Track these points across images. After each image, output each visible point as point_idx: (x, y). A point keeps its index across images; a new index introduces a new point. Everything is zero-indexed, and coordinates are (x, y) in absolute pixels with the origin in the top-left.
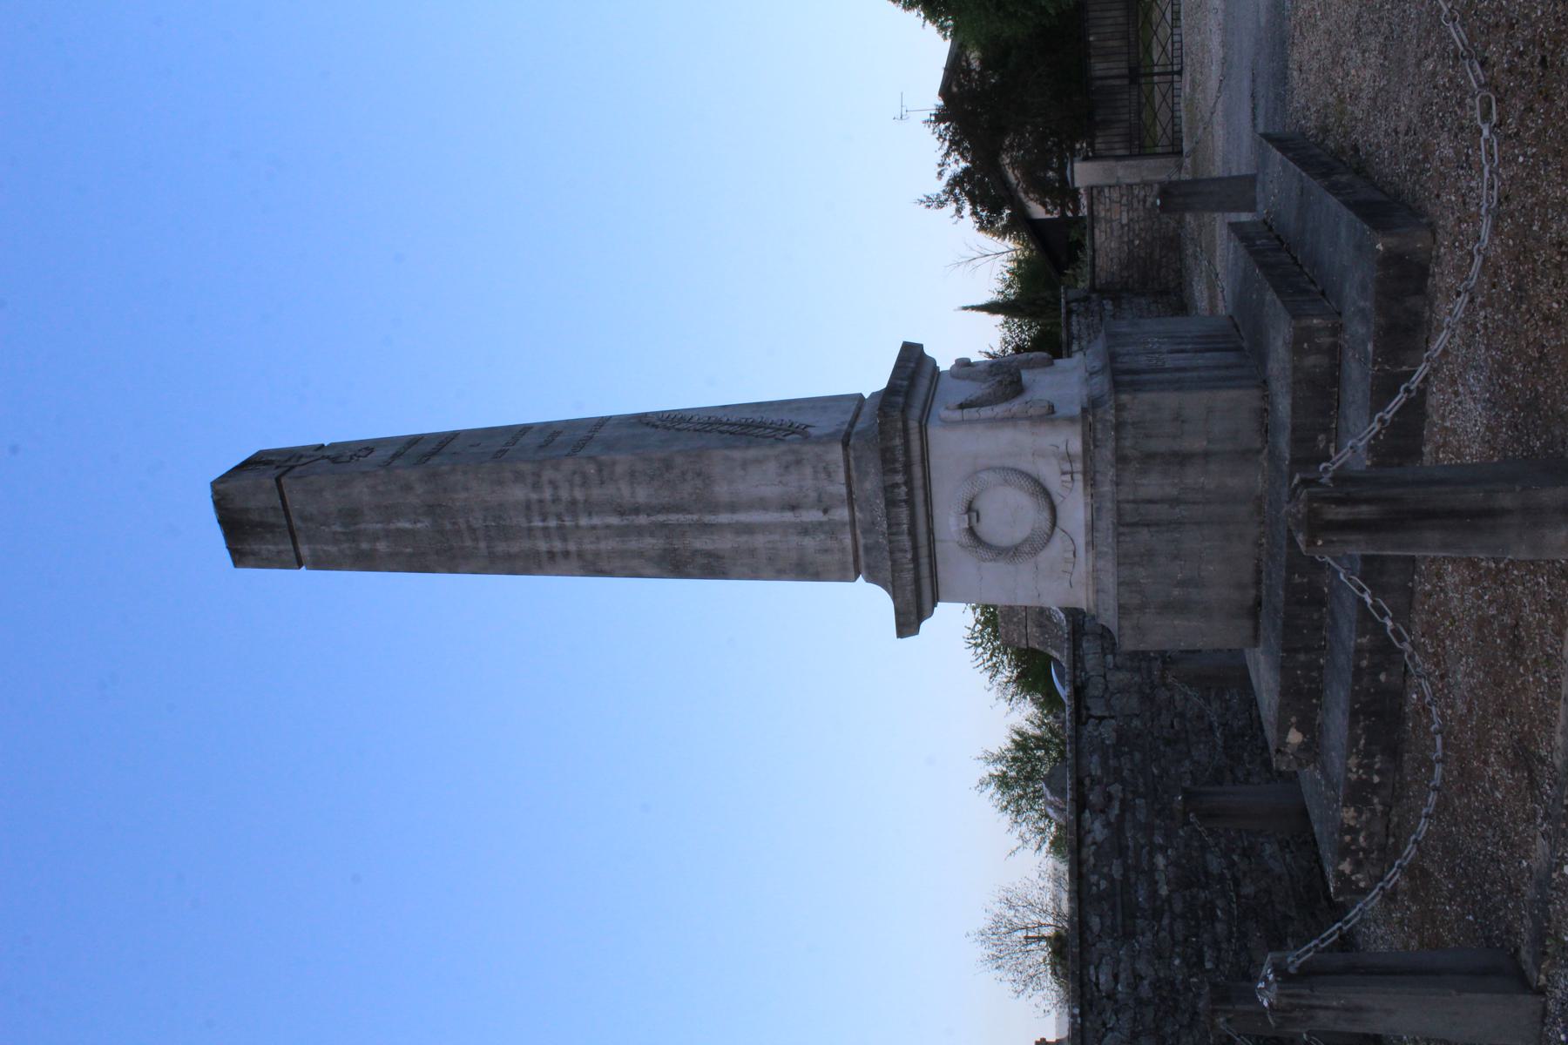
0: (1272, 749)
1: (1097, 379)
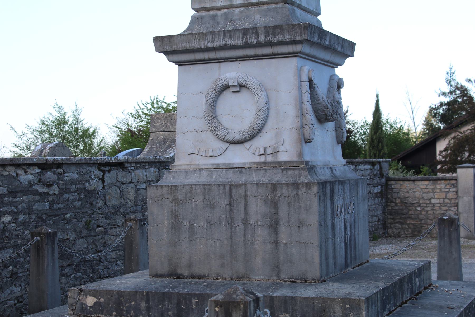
0: (82, 287)
1: (328, 172)
